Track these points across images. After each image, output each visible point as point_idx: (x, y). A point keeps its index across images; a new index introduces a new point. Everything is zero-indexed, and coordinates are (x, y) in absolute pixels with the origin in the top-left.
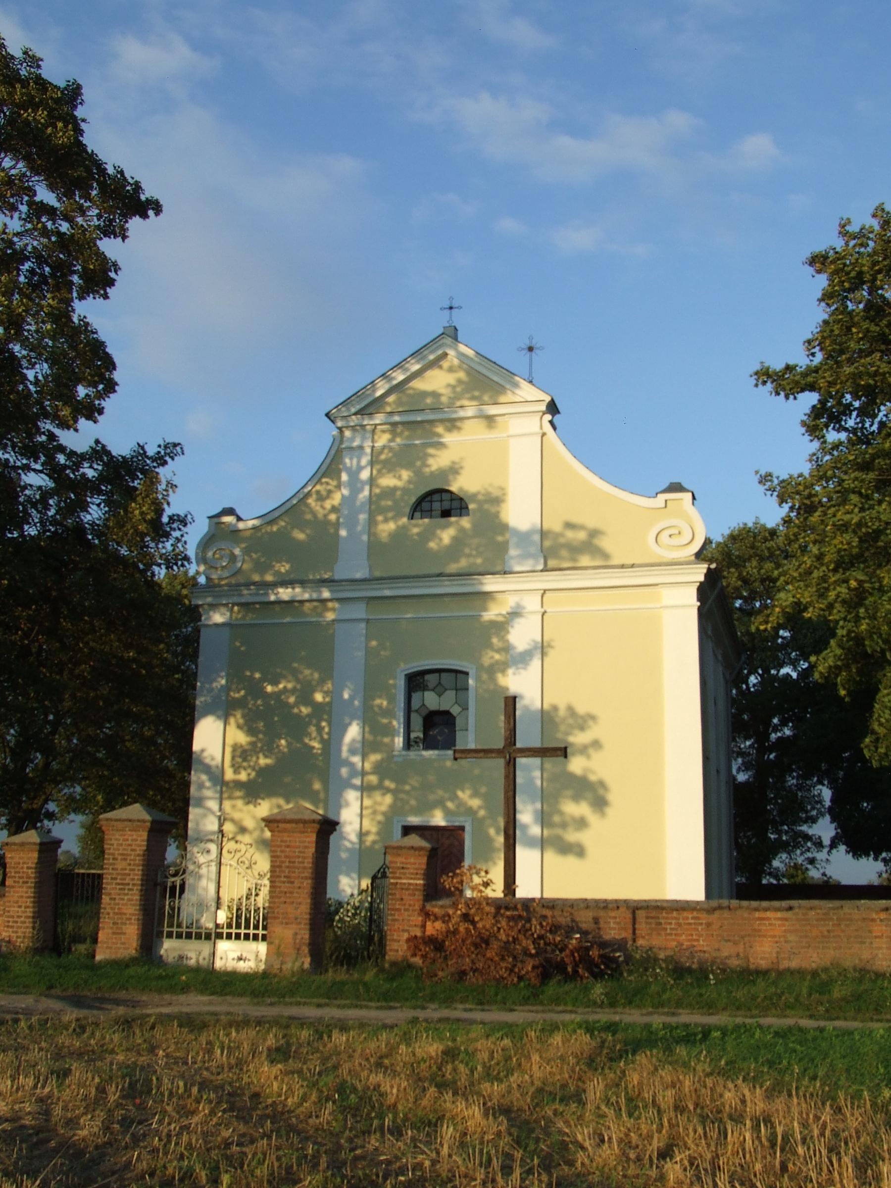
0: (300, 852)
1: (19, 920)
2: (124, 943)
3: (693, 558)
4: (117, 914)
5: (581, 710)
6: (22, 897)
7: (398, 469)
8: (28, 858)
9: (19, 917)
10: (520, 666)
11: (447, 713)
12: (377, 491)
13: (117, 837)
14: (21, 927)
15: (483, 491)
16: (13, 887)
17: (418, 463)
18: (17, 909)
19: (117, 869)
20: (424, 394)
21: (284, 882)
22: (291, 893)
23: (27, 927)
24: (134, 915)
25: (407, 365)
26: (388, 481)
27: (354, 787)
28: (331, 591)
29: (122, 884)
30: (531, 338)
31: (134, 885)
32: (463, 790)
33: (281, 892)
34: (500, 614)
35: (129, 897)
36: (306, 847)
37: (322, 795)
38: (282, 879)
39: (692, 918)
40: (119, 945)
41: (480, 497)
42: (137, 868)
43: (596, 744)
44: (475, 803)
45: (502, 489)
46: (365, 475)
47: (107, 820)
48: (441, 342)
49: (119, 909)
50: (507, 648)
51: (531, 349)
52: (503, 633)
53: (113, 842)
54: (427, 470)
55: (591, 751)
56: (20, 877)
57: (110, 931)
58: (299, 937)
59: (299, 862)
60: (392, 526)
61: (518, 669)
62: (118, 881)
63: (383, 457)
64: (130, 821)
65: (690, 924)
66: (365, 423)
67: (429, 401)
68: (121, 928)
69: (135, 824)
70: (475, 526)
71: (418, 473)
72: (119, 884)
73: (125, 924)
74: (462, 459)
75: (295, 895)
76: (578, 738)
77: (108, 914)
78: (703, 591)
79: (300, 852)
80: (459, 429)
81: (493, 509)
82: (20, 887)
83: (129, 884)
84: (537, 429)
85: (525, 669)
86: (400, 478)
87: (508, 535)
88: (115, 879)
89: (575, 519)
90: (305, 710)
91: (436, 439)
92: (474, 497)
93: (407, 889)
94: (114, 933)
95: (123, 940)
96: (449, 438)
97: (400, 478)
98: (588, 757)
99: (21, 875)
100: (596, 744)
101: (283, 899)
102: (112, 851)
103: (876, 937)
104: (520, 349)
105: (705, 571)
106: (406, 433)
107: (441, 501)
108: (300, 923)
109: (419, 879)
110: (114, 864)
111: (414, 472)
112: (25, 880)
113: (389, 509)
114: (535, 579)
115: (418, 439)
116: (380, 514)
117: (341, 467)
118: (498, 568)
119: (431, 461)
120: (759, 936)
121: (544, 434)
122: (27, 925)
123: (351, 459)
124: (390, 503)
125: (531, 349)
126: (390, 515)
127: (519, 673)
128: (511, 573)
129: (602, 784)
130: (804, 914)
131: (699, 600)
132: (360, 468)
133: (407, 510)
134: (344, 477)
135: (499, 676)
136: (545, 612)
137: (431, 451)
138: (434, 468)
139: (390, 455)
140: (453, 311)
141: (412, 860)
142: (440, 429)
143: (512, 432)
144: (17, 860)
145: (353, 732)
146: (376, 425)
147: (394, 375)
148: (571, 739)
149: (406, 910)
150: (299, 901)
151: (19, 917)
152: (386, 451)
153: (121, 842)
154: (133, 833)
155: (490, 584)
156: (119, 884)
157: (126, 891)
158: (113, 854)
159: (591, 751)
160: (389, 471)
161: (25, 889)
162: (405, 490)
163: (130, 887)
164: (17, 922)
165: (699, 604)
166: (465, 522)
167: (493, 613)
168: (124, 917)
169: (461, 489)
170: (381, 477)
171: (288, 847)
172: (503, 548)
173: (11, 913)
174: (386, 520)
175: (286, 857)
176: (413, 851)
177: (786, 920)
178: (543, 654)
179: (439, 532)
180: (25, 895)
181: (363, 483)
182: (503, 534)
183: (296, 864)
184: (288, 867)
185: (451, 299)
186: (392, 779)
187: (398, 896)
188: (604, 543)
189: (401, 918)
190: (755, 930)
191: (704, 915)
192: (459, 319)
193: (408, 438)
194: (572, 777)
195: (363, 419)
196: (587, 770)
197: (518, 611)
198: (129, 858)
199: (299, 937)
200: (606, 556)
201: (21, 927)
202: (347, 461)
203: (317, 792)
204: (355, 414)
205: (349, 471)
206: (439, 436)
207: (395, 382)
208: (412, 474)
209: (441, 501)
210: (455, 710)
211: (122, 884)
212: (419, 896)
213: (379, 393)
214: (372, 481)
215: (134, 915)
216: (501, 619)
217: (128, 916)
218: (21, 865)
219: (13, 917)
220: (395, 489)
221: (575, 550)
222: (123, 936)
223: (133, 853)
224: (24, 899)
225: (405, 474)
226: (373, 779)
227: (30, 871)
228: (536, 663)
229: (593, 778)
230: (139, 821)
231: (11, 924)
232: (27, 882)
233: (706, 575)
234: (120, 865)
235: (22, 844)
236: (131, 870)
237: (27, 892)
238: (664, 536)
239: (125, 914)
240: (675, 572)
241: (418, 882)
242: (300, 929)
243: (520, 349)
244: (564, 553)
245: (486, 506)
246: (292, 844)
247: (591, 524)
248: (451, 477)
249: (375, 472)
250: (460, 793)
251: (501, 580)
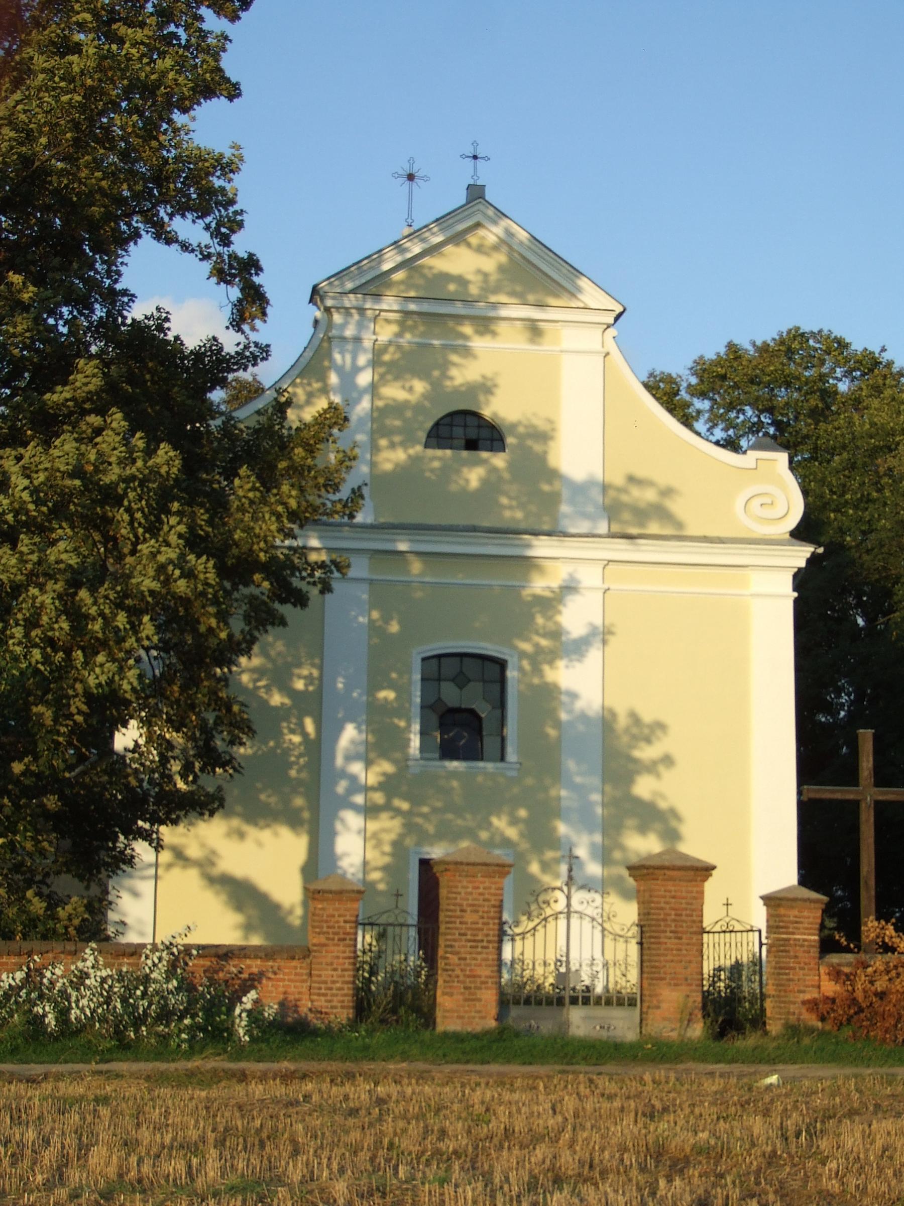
0: (688, 904)
1: (334, 986)
2: (479, 1012)
3: (787, 536)
4: (469, 976)
5: (647, 717)
6: (338, 957)
7: (408, 376)
8: (346, 910)
9: (334, 982)
10: (574, 657)
11: (472, 712)
12: (380, 404)
13: (465, 884)
14: (337, 995)
15: (525, 422)
17: (436, 373)
18: (330, 973)
19: (466, 923)
20: (446, 277)
22: (680, 950)
23: (345, 995)
24: (491, 977)
25: (427, 234)
26: (394, 392)
27: (355, 808)
28: (320, 538)
29: (474, 941)
30: (411, 161)
31: (489, 942)
32: (499, 817)
34: (549, 588)
35: (484, 956)
37: (306, 815)
38: (668, 934)
40: (473, 1014)
41: (521, 429)
42: (491, 922)
43: (668, 760)
44: (512, 833)
45: (550, 421)
46: (364, 379)
48: (475, 208)
49: (471, 970)
50: (556, 634)
51: (411, 177)
52: (550, 613)
53: (459, 890)
54: (448, 383)
55: (661, 768)
56: (334, 934)
57: (461, 997)
58: (691, 1000)
59: (687, 915)
60: (400, 455)
61: (571, 660)
62: (469, 937)
63: (387, 357)
64: (486, 864)
66: (368, 306)
67: (452, 287)
68: (475, 994)
69: (491, 869)
70: (511, 466)
71: (436, 386)
72: (470, 941)
73: (480, 988)
74: (497, 374)
75: (684, 952)
76: (645, 753)
77: (458, 976)
78: (801, 580)
79: (688, 904)
80: (494, 334)
81: (537, 448)
82: (334, 945)
83: (482, 941)
84: (598, 347)
85: (579, 661)
86: (411, 390)
87: (557, 485)
88: (465, 935)
89: (641, 472)
90: (277, 699)
91: (460, 342)
92: (513, 426)
93: (802, 946)
94: (466, 1000)
95: (478, 1008)
96: (479, 343)
97: (411, 390)
98: (658, 776)
99: (336, 930)
100: (668, 760)
102: (458, 901)
104: (397, 176)
105: (808, 555)
106: (422, 328)
107: (465, 426)
108: (691, 985)
109: (814, 935)
110: (462, 917)
111: (431, 384)
112: (342, 936)
113: (397, 431)
114: (601, 546)
115: (438, 339)
116: (383, 436)
117: (326, 363)
118: (546, 527)
119: (454, 372)
121: (607, 354)
122: (346, 991)
123: (342, 353)
124: (398, 423)
125: (411, 177)
126: (397, 439)
127: (574, 667)
128: (566, 535)
129: (673, 813)
131: (795, 589)
132: (356, 370)
133: (422, 435)
134: (333, 379)
135: (546, 668)
137: (454, 358)
138: (459, 381)
139: (397, 356)
140: (479, 162)
141: (806, 914)
142: (467, 329)
143: (565, 345)
144: (331, 912)
145: (350, 734)
146: (381, 311)
147: (408, 245)
148: (637, 754)
149: (802, 969)
150: (688, 958)
151: (334, 982)
152: (391, 349)
153: (469, 890)
154: (486, 880)
155: (541, 548)
156: (470, 941)
157: (479, 950)
158: (461, 905)
159: (661, 768)
160: (397, 378)
161: (341, 948)
162: (418, 408)
163: (485, 944)
164: (331, 989)
165: (796, 594)
166: (499, 461)
167: (539, 585)
168: (478, 980)
169: (495, 414)
170: (384, 385)
171: (674, 897)
172: (554, 499)
173: (323, 978)
174: (392, 446)
176: (808, 904)
178: (604, 642)
179: (465, 470)
180: (341, 955)
181: (362, 392)
182: (550, 482)
183: (684, 918)
184: (674, 920)
185: (475, 144)
186: (405, 797)
187: (792, 954)
188: (676, 507)
189: (796, 978)
192: (485, 175)
193: (422, 335)
194: (638, 802)
195: (364, 301)
196: (657, 794)
197: (573, 585)
198: (481, 909)
199: (691, 1000)
200: (679, 525)
201: (337, 995)
202: (337, 357)
203: (300, 810)
204: (353, 291)
205: (340, 371)
206: (466, 337)
207: (409, 255)
208: (428, 387)
209: (465, 426)
210: (484, 710)
211: (474, 941)
212: (815, 952)
213: (386, 267)
214: (373, 388)
215: (491, 977)
216: (547, 594)
217: (483, 979)
218: (337, 918)
219: (326, 982)
220: (405, 405)
221: (642, 514)
222: (478, 1004)
223: (486, 903)
224: (341, 961)
225: (420, 387)
226: (378, 798)
227: (348, 925)
228: (594, 655)
229: (663, 805)
230: (498, 865)
231: (323, 991)
232: (344, 939)
233: (809, 561)
234: (470, 917)
236: (484, 924)
237: (344, 952)
238: (756, 502)
239: (480, 977)
240: (776, 553)
241: (813, 938)
242: (691, 991)
243: (397, 176)
244: (626, 516)
245: (529, 443)
246: (678, 894)
247: (663, 480)
248: (482, 398)
249: (376, 377)
250: (495, 821)
251: (556, 543)
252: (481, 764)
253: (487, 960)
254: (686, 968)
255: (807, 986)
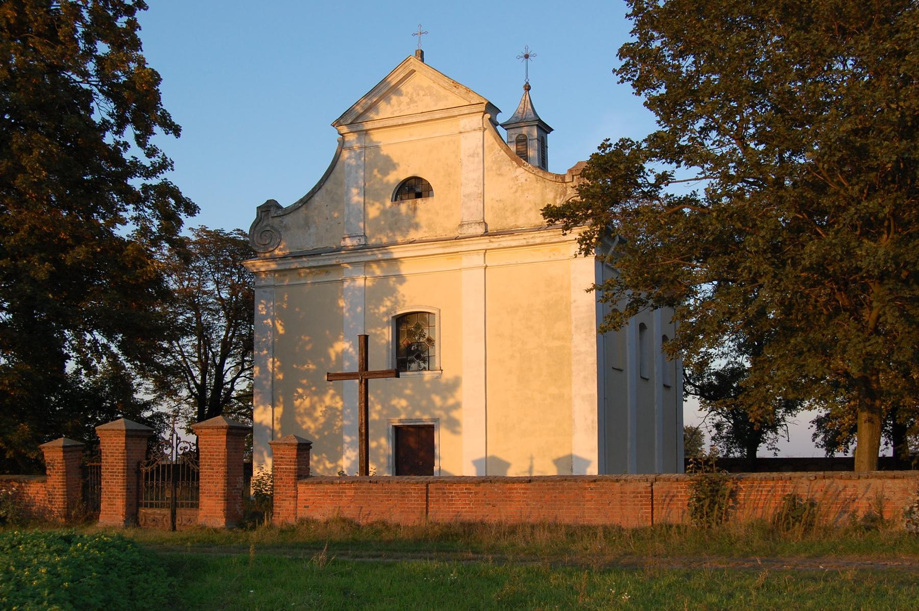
2: (115, 511)
16: (50, 475)
21: (207, 469)
30: (526, 48)
33: (206, 476)
36: (220, 445)
39: (466, 489)
47: (100, 430)
51: (527, 57)
64: (113, 430)
65: (465, 493)
88: (108, 469)
93: (285, 472)
94: (109, 504)
101: (207, 480)
103: (587, 501)
104: (519, 58)
120: (510, 501)
125: (527, 57)
130: (539, 486)
136: (487, 266)
175: (208, 452)
177: (527, 489)
184: (210, 459)
190: (507, 497)
191: (473, 487)
212: (292, 476)
230: (118, 430)
235: (53, 447)
243: (519, 58)
252: (408, 373)
253: (118, 483)
254: (216, 486)
255: (287, 497)
